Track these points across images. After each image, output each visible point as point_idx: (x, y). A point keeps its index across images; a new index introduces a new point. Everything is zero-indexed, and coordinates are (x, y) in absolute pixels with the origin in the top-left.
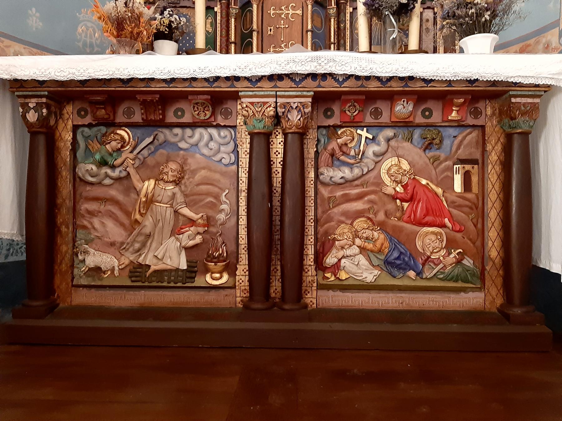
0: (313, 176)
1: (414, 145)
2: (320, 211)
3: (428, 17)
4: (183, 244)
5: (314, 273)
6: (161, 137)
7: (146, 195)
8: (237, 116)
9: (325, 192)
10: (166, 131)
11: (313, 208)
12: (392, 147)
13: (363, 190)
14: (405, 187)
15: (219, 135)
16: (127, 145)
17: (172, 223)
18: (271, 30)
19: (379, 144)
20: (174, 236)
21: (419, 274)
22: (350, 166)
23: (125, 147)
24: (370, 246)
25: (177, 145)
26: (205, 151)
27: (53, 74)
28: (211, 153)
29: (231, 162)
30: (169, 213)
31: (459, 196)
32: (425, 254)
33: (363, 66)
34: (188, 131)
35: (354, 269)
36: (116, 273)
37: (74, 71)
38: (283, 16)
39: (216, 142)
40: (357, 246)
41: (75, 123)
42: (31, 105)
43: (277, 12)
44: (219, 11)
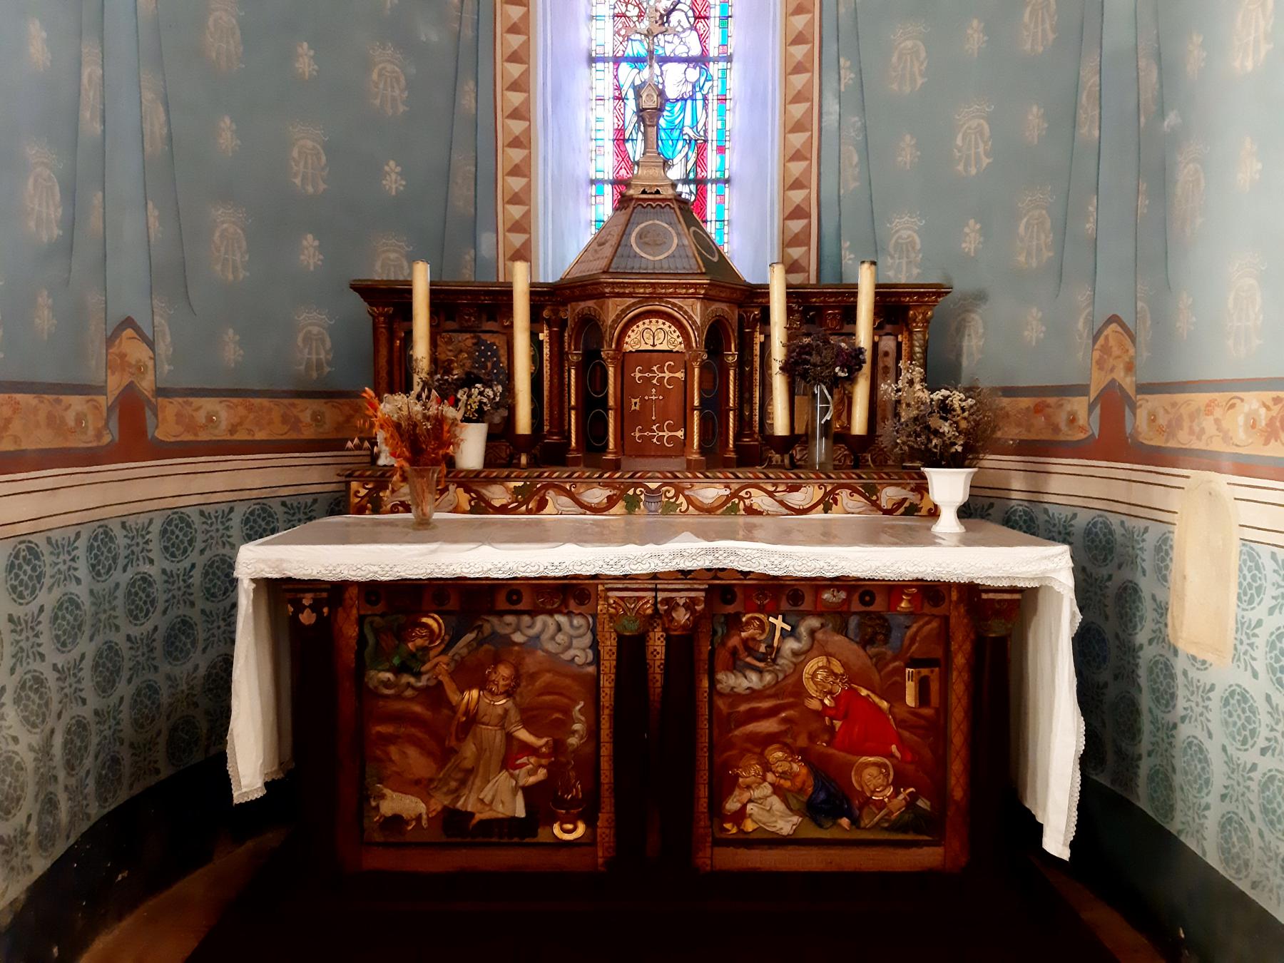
0: (707, 685)
1: (850, 639)
2: (716, 732)
3: (886, 349)
4: (521, 783)
5: (708, 823)
6: (487, 629)
7: (467, 713)
8: (598, 600)
9: (721, 703)
10: (494, 620)
11: (707, 731)
12: (818, 641)
13: (779, 702)
14: (836, 699)
15: (571, 625)
16: (437, 639)
17: (503, 751)
18: (636, 403)
19: (798, 639)
20: (507, 770)
21: (855, 822)
22: (760, 671)
23: (435, 642)
24: (787, 784)
25: (510, 638)
26: (551, 647)
27: (346, 572)
28: (560, 649)
29: (588, 661)
30: (499, 737)
31: (912, 712)
32: (863, 792)
33: (776, 562)
34: (526, 619)
35: (765, 817)
36: (424, 822)
37: (376, 569)
38: (655, 382)
39: (566, 633)
40: (770, 783)
41: (362, 612)
42: (306, 602)
43: (646, 375)
44: (546, 339)
